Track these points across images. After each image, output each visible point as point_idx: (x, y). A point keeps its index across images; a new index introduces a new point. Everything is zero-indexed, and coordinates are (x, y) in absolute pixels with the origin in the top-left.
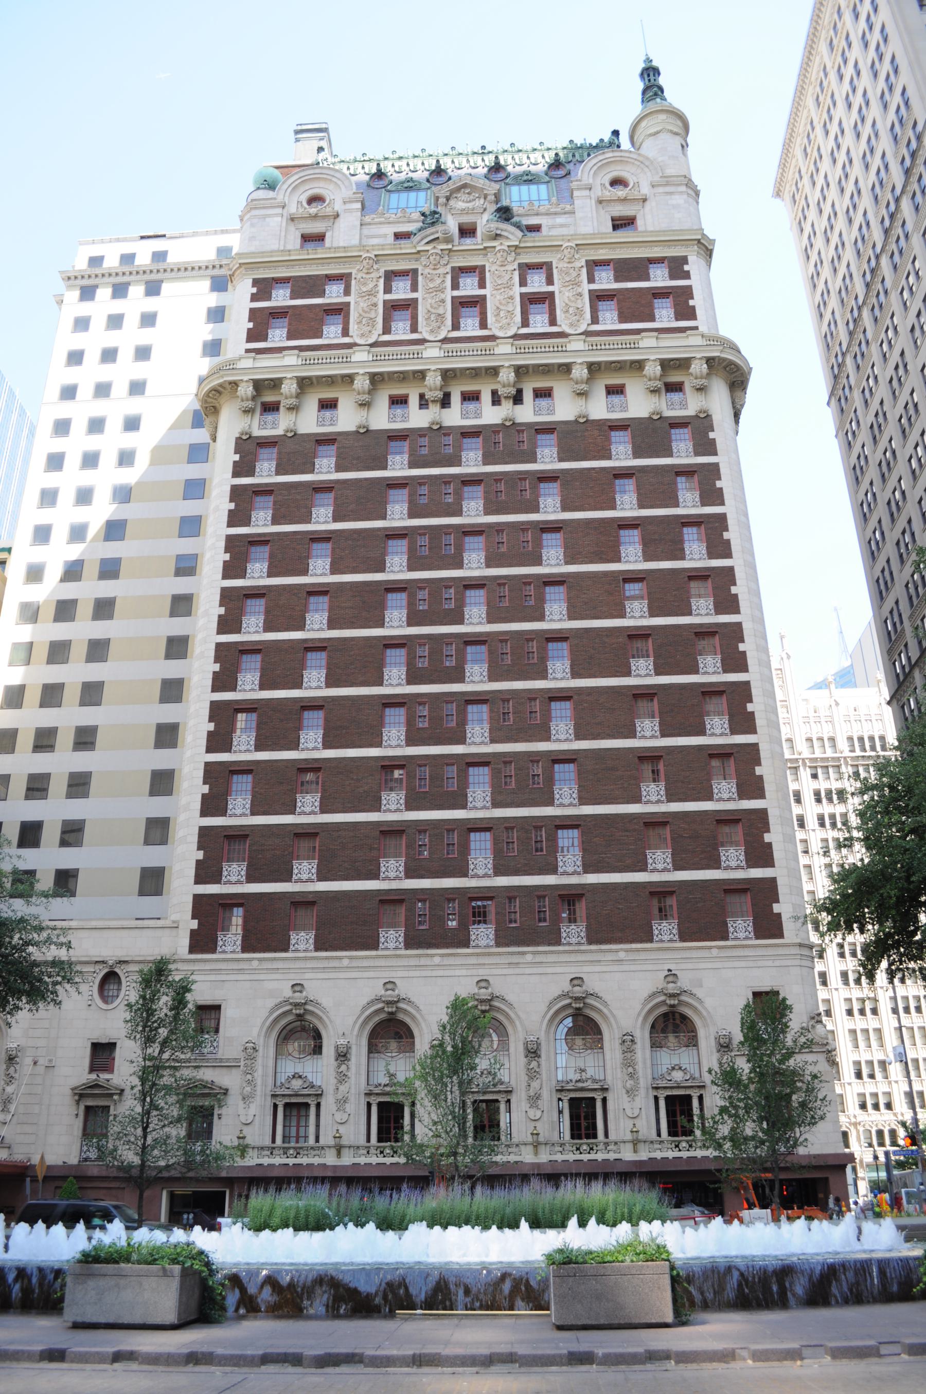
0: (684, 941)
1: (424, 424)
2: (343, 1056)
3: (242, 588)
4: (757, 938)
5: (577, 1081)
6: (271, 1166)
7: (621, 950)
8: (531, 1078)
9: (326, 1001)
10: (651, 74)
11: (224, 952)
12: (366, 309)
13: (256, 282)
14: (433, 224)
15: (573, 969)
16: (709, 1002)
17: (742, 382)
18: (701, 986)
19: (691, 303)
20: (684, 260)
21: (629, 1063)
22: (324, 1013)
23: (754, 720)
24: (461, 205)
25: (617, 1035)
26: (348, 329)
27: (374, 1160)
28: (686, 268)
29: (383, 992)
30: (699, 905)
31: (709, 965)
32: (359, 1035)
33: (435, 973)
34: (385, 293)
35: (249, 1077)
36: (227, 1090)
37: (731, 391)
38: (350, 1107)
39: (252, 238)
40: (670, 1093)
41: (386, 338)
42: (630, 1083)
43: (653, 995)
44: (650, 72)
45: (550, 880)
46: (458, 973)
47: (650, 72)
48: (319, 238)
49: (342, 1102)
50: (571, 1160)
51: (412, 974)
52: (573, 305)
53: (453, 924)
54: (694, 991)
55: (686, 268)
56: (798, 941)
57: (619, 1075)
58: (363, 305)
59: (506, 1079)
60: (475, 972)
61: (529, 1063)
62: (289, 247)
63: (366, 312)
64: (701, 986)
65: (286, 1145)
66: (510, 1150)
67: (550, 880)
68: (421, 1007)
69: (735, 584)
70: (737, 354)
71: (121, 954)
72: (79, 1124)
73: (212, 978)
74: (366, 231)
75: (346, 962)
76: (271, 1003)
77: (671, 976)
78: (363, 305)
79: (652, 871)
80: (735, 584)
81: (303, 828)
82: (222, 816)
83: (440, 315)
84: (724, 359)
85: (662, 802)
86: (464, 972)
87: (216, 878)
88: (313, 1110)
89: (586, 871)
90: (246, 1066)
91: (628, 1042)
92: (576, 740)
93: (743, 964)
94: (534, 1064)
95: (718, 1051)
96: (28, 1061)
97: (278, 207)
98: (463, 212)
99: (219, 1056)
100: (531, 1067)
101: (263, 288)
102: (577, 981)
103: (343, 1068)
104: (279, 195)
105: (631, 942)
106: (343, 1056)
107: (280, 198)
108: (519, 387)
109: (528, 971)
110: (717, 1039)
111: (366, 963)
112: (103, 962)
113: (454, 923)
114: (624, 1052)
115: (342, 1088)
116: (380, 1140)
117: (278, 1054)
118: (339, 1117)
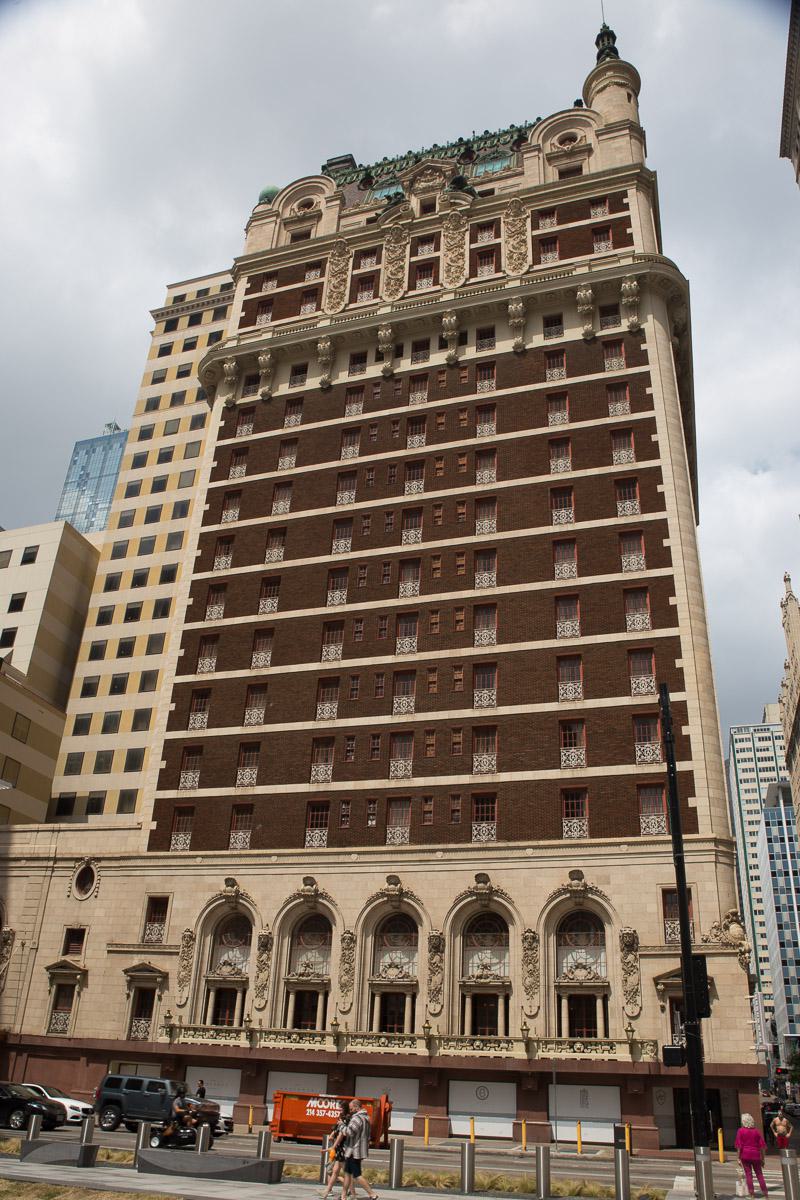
0: (593, 837)
1: (379, 373)
2: (437, 945)
3: (216, 532)
4: (592, 837)
5: (478, 977)
6: (558, 1061)
7: (529, 848)
8: (433, 972)
9: (254, 895)
10: (606, 39)
11: (176, 850)
12: (336, 285)
13: (250, 280)
14: (396, 204)
15: (481, 866)
16: (615, 900)
17: (680, 296)
18: (609, 883)
19: (629, 231)
20: (625, 194)
21: (529, 960)
22: (418, 904)
23: (676, 612)
24: (423, 185)
25: (520, 931)
26: (500, 266)
27: (566, 1054)
28: (625, 201)
29: (302, 886)
30: (611, 801)
31: (618, 862)
32: (281, 928)
33: (351, 870)
34: (532, 230)
35: (185, 962)
36: (167, 974)
37: (668, 309)
38: (444, 998)
39: (250, 245)
40: (572, 993)
41: (472, 280)
42: (529, 980)
43: (559, 893)
44: (606, 38)
45: (464, 779)
46: (373, 869)
47: (606, 38)
48: (307, 235)
49: (435, 993)
50: (492, 1057)
51: (332, 870)
52: (517, 251)
53: (372, 823)
54: (600, 888)
55: (625, 201)
56: (713, 836)
57: (520, 971)
58: (334, 281)
59: (603, 975)
60: (384, 869)
61: (626, 957)
62: (550, 181)
63: (395, 274)
64: (609, 883)
65: (474, 1037)
66: (549, 1046)
67: (464, 779)
68: (337, 902)
69: (661, 483)
70: (671, 269)
71: (95, 852)
72: (50, 999)
73: (164, 873)
74: (343, 222)
75: (274, 859)
76: (209, 896)
77: (576, 875)
78: (334, 281)
79: (566, 768)
80: (661, 483)
81: (480, 722)
82: (183, 730)
83: (398, 280)
84: (656, 275)
85: (579, 699)
86: (378, 869)
87: (175, 785)
88: (501, 1001)
89: (500, 770)
90: (184, 952)
91: (531, 940)
92: (582, 635)
93: (654, 860)
94: (437, 958)
95: (622, 950)
96: (17, 943)
97: (535, 150)
98: (425, 190)
99: (164, 943)
100: (434, 961)
101: (256, 284)
102: (482, 878)
103: (437, 958)
104: (276, 206)
105: (540, 839)
106: (265, 944)
107: (275, 208)
108: (464, 329)
109: (437, 868)
110: (622, 937)
111: (550, 852)
112: (82, 859)
113: (374, 823)
114: (344, 949)
115: (261, 975)
116: (571, 1034)
117: (466, 945)
118: (630, 1010)
